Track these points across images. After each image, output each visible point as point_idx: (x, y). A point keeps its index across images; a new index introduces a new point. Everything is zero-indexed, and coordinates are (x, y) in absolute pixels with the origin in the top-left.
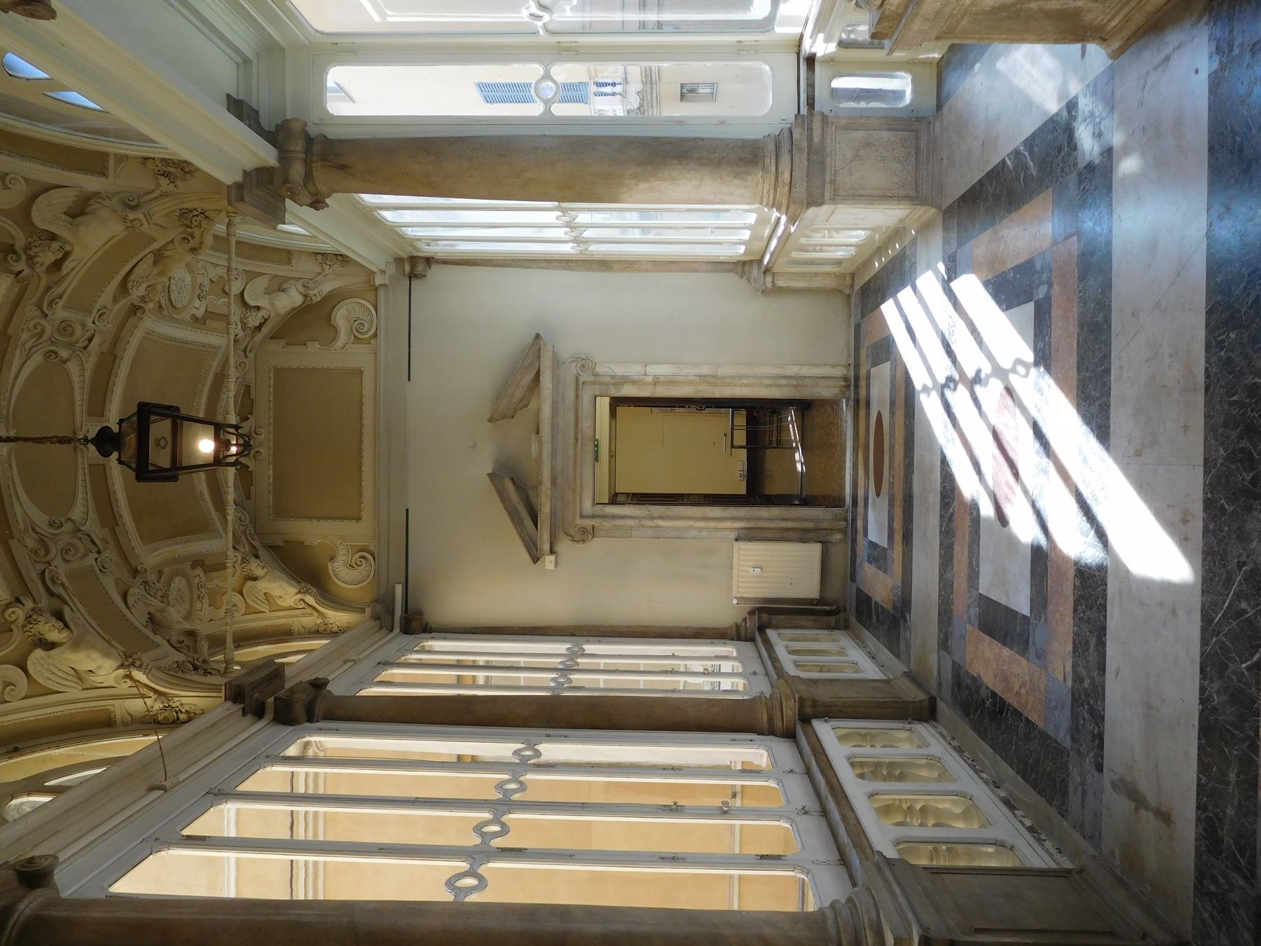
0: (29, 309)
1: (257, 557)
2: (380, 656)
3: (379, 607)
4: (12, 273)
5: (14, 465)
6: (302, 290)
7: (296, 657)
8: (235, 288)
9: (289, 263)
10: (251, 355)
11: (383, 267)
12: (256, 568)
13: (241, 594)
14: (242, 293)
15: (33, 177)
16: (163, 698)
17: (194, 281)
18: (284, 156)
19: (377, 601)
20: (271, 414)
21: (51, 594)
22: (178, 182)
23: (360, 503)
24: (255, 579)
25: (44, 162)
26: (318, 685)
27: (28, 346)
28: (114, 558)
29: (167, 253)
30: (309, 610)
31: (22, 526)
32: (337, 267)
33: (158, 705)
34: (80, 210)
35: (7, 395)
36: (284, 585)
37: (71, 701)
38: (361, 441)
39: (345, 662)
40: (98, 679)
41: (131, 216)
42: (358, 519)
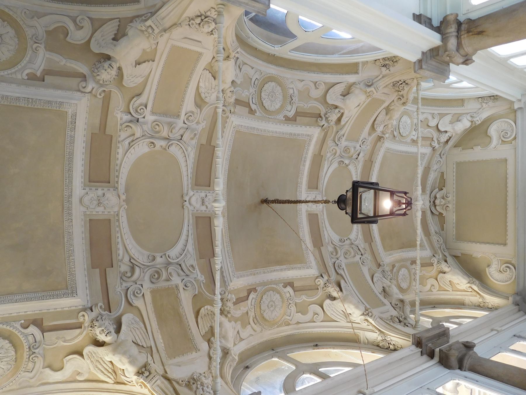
0: (329, 142)
1: (446, 261)
2: (516, 330)
3: (518, 298)
4: (320, 126)
5: (325, 213)
6: (470, 119)
7: (460, 324)
8: (433, 123)
9: (463, 106)
10: (444, 157)
11: (520, 98)
12: (444, 267)
13: (437, 280)
14: (437, 125)
15: (327, 81)
16: (383, 335)
17: (412, 122)
18: (444, 39)
19: (517, 294)
20: (454, 186)
21: (338, 273)
22: (391, 68)
23: (506, 235)
24: (445, 273)
25: (332, 73)
26: (469, 346)
27: (330, 159)
28: (369, 258)
29: (392, 108)
30: (475, 293)
31: (327, 241)
32: (491, 103)
33: (380, 338)
34: (346, 94)
35: (322, 182)
36: (460, 278)
37: (341, 327)
38: (506, 200)
39: (492, 330)
40: (354, 319)
41: (369, 90)
42: (505, 244)
